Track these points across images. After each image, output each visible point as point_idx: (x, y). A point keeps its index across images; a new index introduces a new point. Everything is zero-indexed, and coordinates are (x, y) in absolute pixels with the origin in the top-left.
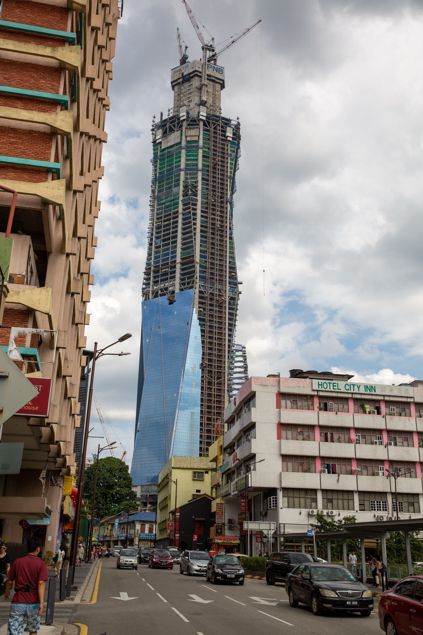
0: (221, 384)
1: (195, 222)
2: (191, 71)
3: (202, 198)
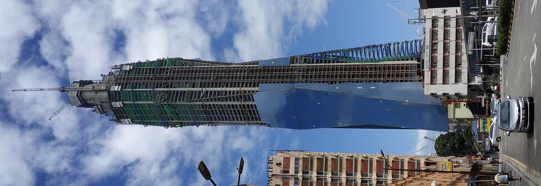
0: (375, 67)
1: (247, 92)
2: (77, 99)
3: (186, 87)
